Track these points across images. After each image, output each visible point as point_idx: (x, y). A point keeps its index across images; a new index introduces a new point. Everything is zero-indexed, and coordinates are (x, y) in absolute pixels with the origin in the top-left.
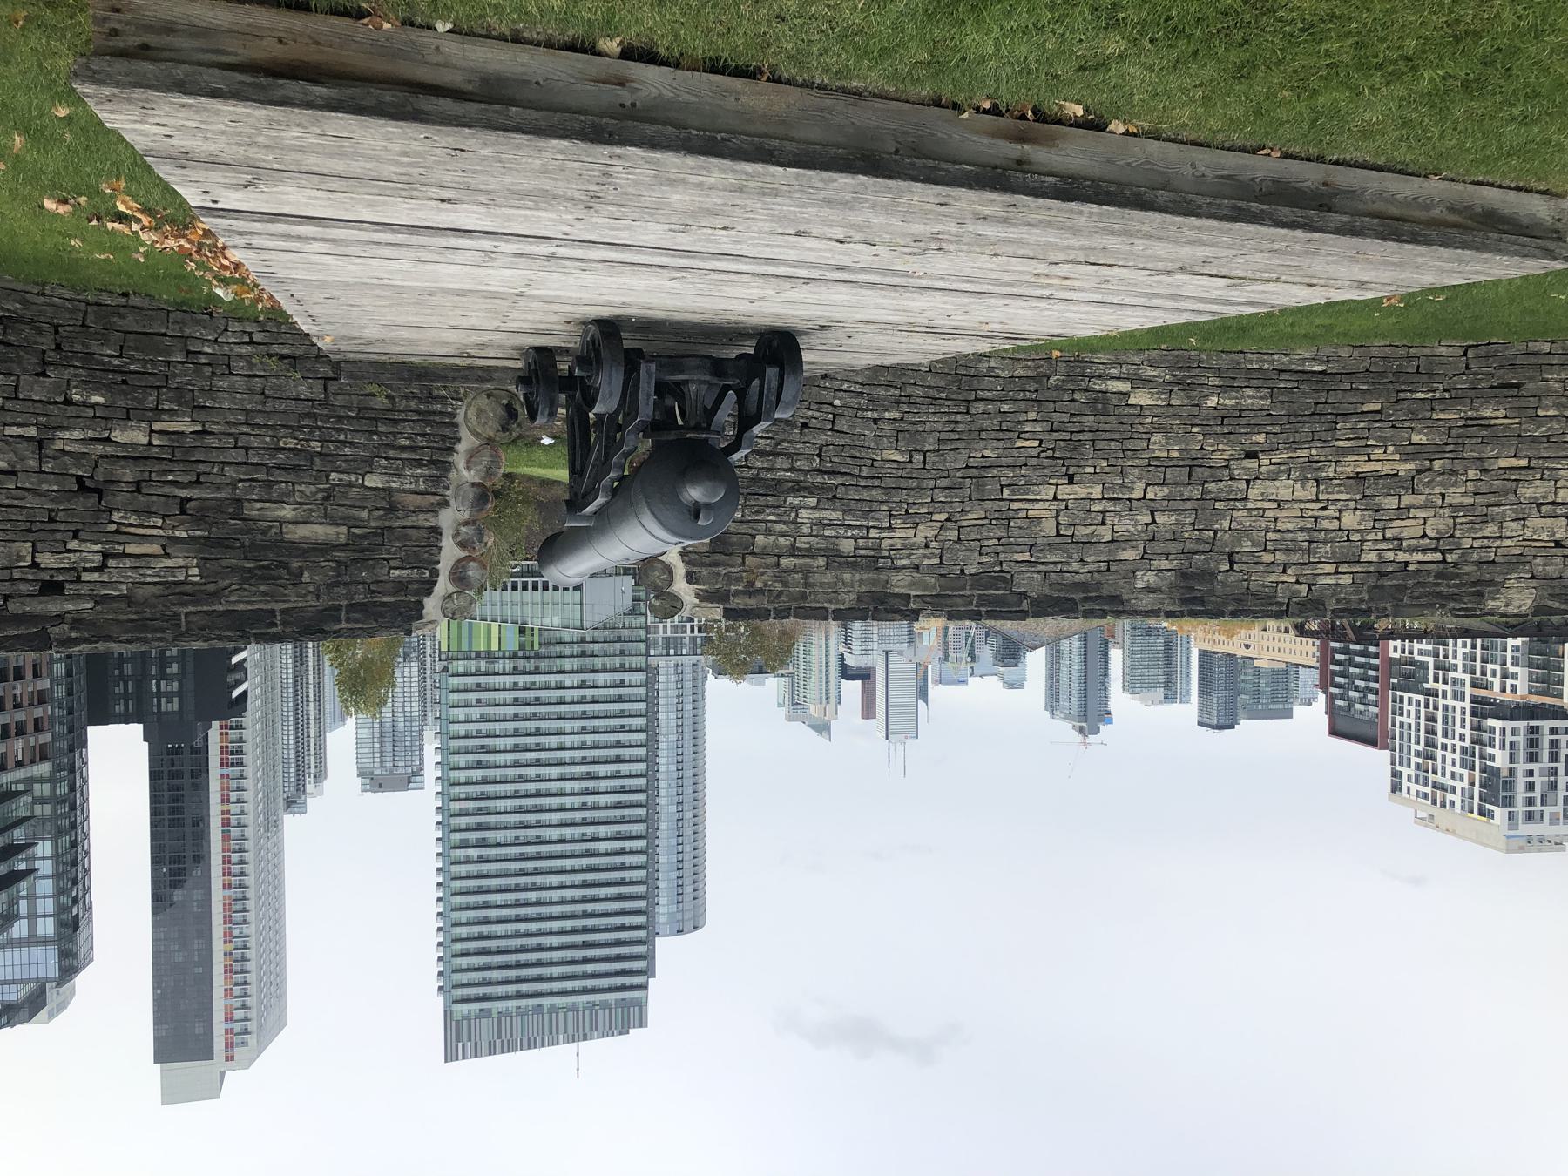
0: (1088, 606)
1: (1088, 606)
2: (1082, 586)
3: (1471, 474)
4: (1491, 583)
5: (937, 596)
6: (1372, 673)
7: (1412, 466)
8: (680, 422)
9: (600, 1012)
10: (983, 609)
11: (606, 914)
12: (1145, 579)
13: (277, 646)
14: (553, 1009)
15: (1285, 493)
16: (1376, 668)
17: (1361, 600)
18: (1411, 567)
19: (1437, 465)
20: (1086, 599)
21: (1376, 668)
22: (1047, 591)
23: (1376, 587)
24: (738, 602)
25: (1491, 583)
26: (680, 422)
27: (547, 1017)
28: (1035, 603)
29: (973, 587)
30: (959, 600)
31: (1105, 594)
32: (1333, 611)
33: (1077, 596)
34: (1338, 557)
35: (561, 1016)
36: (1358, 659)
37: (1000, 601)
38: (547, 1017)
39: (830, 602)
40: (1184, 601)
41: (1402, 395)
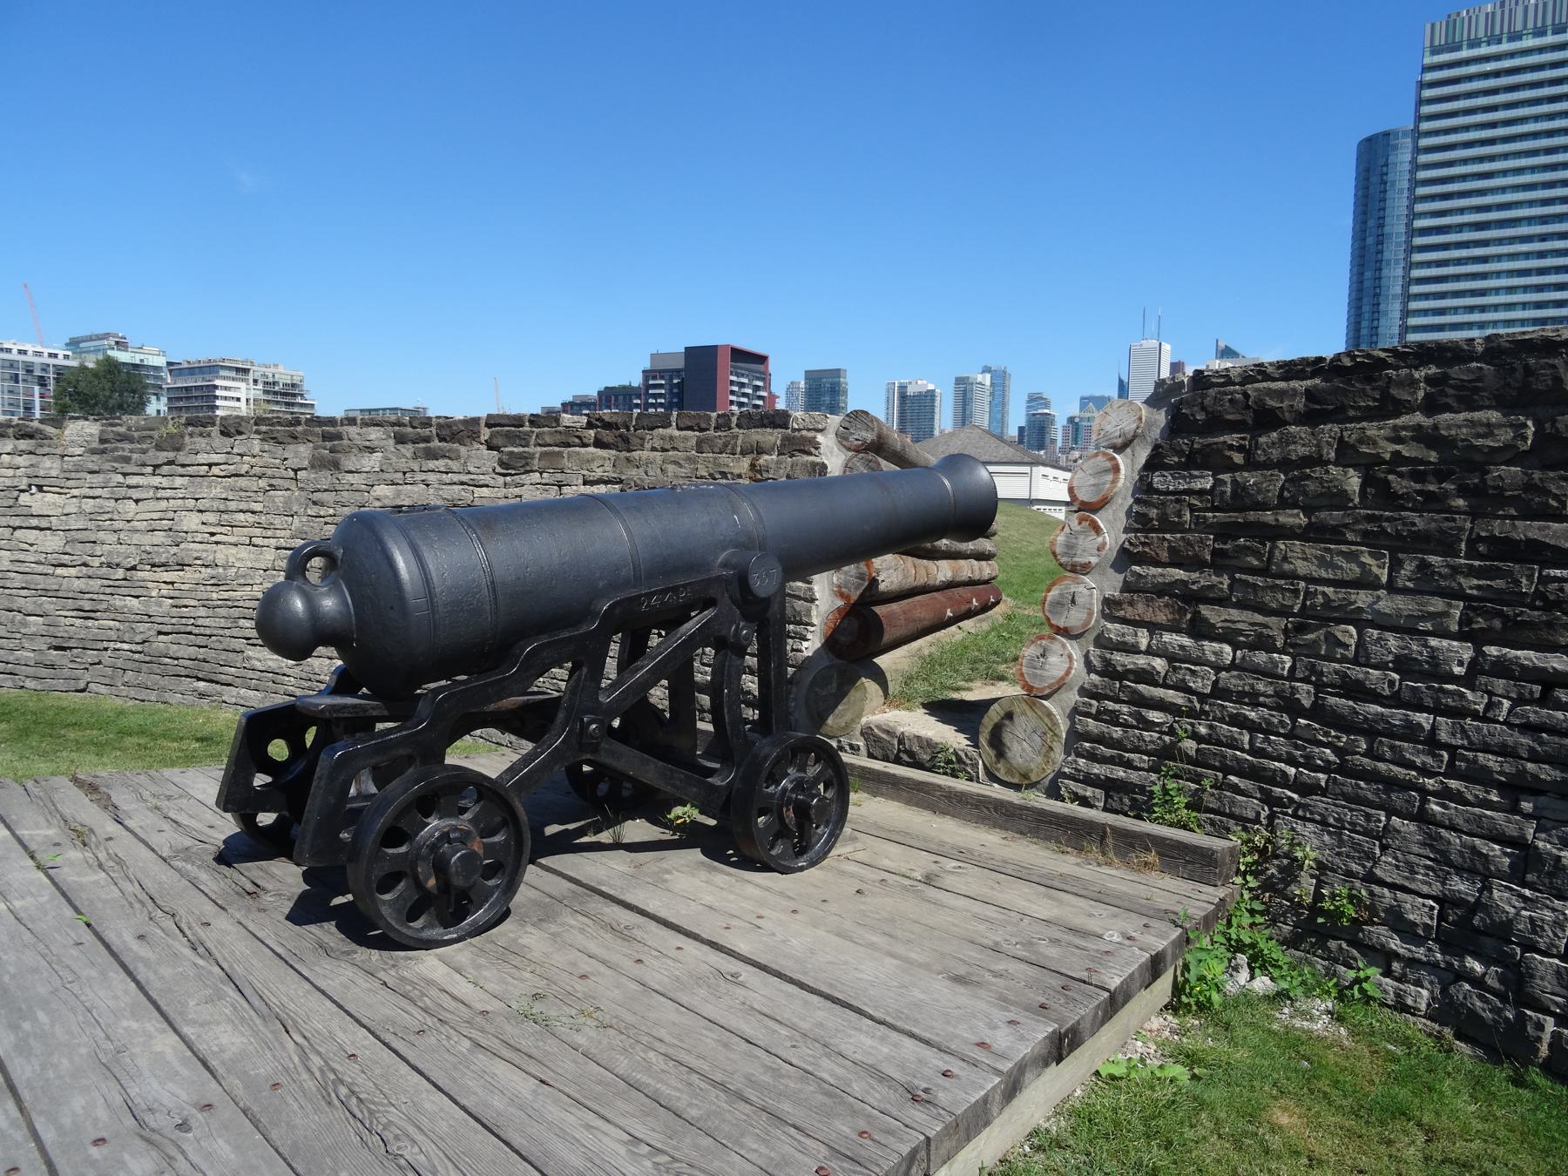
0: (426, 432)
1: (426, 432)
2: (432, 455)
3: (96, 562)
4: (93, 452)
5: (569, 445)
6: (735, 388)
7: (140, 574)
8: (551, 830)
9: (1481, 34)
10: (527, 428)
11: (1465, 161)
12: (372, 462)
13: (852, 809)
14: (1540, 33)
15: (244, 552)
16: (732, 393)
17: (191, 435)
18: (150, 470)
19: (120, 573)
20: (427, 440)
21: (732, 393)
22: (463, 449)
23: (178, 450)
24: (772, 436)
25: (93, 452)
26: (551, 830)
27: (1549, 22)
28: (474, 436)
29: (532, 456)
30: (548, 440)
31: (410, 446)
32: (213, 424)
33: (436, 443)
34: (205, 482)
35: (1530, 25)
36: (745, 400)
37: (512, 439)
38: (1549, 22)
39: (671, 438)
40: (339, 437)
41: (139, 648)
